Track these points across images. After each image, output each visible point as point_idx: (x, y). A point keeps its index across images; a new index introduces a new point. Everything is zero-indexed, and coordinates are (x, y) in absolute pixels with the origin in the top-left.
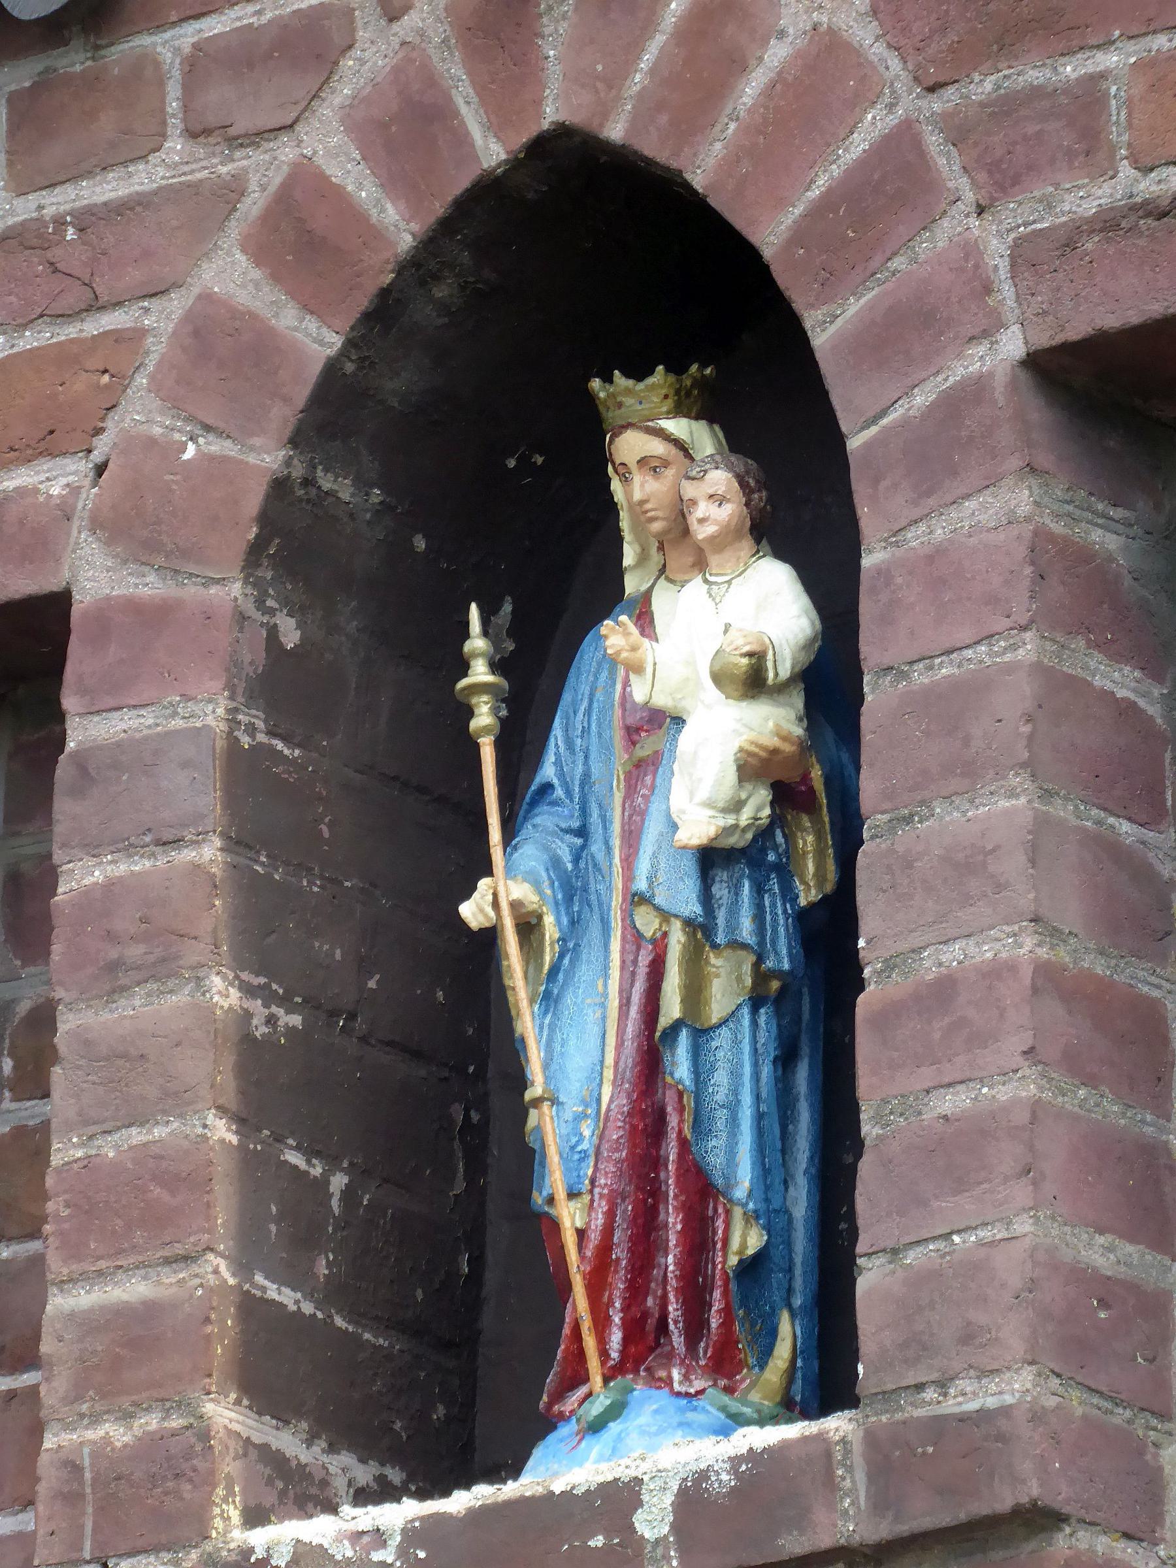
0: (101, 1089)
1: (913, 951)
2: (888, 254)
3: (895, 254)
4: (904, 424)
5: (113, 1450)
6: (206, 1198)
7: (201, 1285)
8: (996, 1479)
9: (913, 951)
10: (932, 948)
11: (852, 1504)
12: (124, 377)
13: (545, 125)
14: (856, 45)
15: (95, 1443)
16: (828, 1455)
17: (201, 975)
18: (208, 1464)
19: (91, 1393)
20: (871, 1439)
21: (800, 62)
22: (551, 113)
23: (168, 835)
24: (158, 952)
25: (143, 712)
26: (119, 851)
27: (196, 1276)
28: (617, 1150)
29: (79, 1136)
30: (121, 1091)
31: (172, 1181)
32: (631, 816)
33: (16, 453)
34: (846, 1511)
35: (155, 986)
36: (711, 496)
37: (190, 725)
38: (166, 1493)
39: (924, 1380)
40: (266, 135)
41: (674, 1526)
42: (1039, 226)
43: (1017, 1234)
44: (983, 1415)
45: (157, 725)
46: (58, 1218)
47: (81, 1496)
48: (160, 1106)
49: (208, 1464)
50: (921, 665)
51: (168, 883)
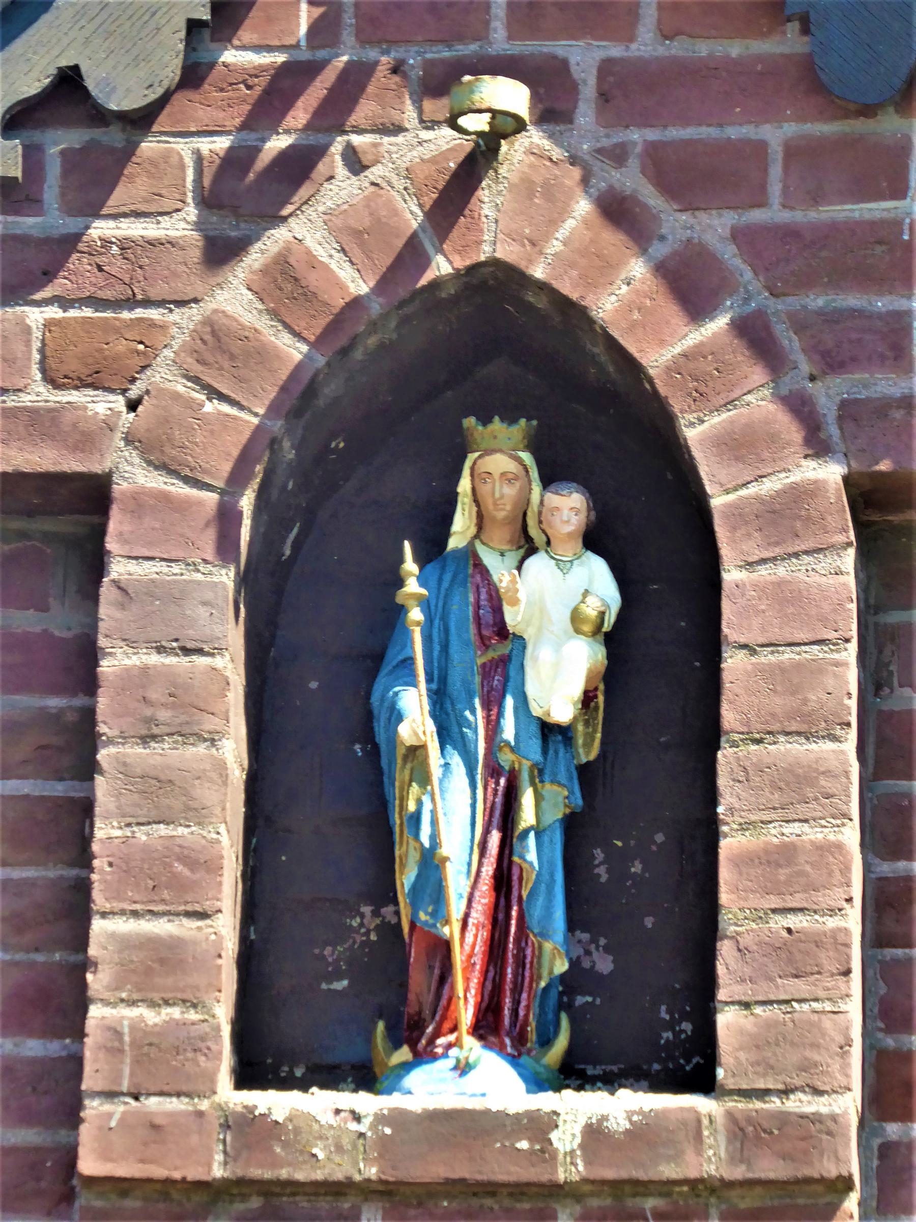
0: (136, 796)
1: (762, 822)
2: (745, 391)
3: (749, 392)
4: (758, 498)
5: (146, 1025)
6: (218, 879)
7: (215, 933)
8: (825, 1157)
9: (762, 822)
10: (776, 824)
11: (715, 1154)
12: (156, 349)
13: (483, 258)
14: (720, 257)
15: (132, 1019)
16: (699, 1121)
17: (216, 738)
18: (217, 1047)
19: (129, 987)
20: (730, 1115)
21: (678, 258)
22: (484, 253)
23: (190, 645)
24: (184, 718)
25: (173, 565)
26: (152, 648)
27: (211, 926)
28: (484, 898)
29: (119, 823)
30: (152, 800)
31: (192, 863)
32: (489, 692)
33: (70, 381)
34: (710, 1158)
35: (180, 738)
36: (572, 509)
37: (208, 579)
38: (187, 1060)
39: (771, 1086)
40: (266, 219)
41: (581, 1146)
42: (858, 396)
43: (841, 1010)
44: (816, 1118)
45: (182, 574)
46: (102, 871)
47: (121, 1051)
48: (183, 815)
49: (217, 1047)
50: (769, 649)
51: (191, 675)
